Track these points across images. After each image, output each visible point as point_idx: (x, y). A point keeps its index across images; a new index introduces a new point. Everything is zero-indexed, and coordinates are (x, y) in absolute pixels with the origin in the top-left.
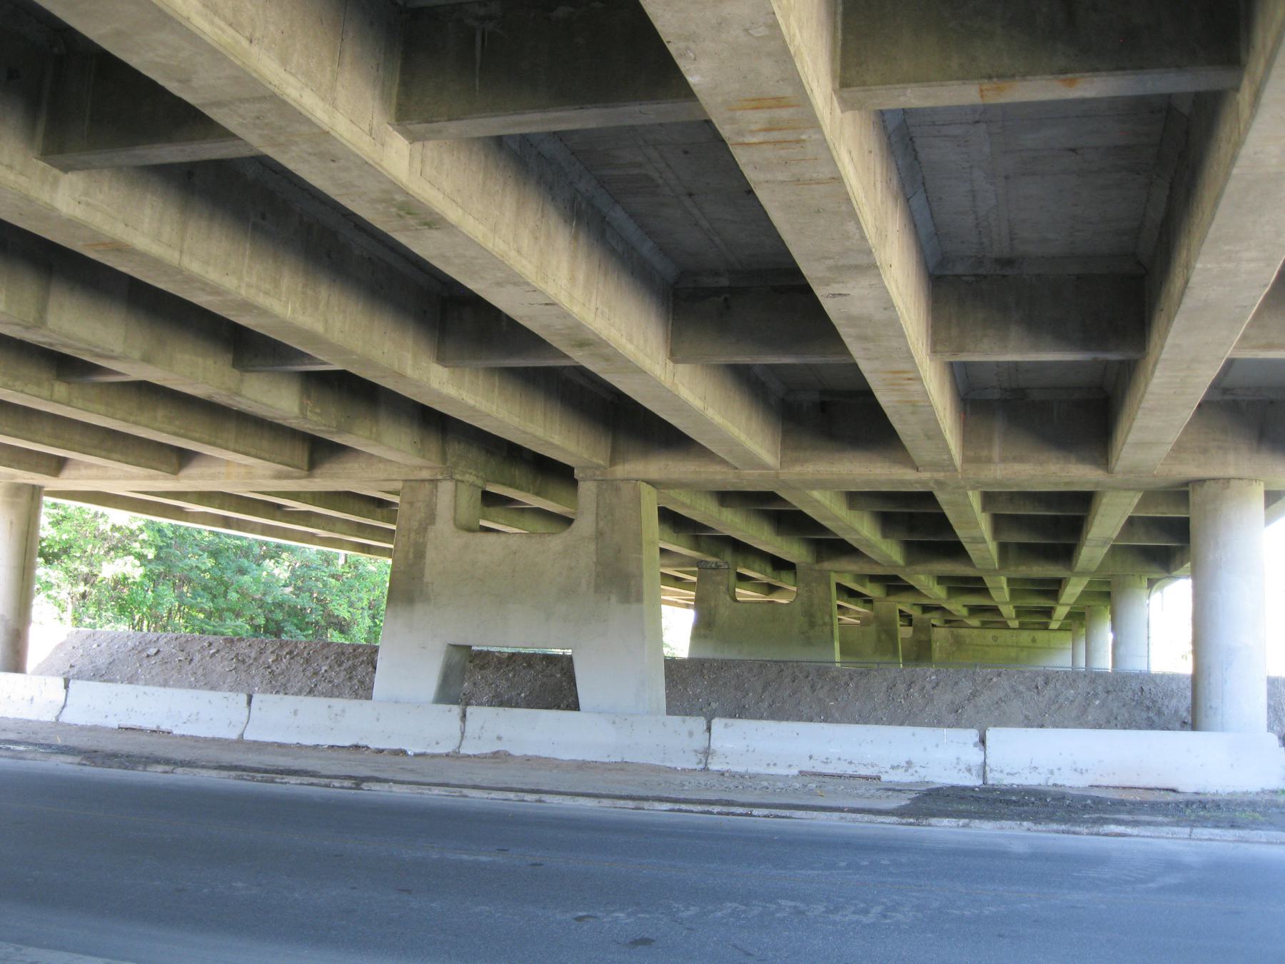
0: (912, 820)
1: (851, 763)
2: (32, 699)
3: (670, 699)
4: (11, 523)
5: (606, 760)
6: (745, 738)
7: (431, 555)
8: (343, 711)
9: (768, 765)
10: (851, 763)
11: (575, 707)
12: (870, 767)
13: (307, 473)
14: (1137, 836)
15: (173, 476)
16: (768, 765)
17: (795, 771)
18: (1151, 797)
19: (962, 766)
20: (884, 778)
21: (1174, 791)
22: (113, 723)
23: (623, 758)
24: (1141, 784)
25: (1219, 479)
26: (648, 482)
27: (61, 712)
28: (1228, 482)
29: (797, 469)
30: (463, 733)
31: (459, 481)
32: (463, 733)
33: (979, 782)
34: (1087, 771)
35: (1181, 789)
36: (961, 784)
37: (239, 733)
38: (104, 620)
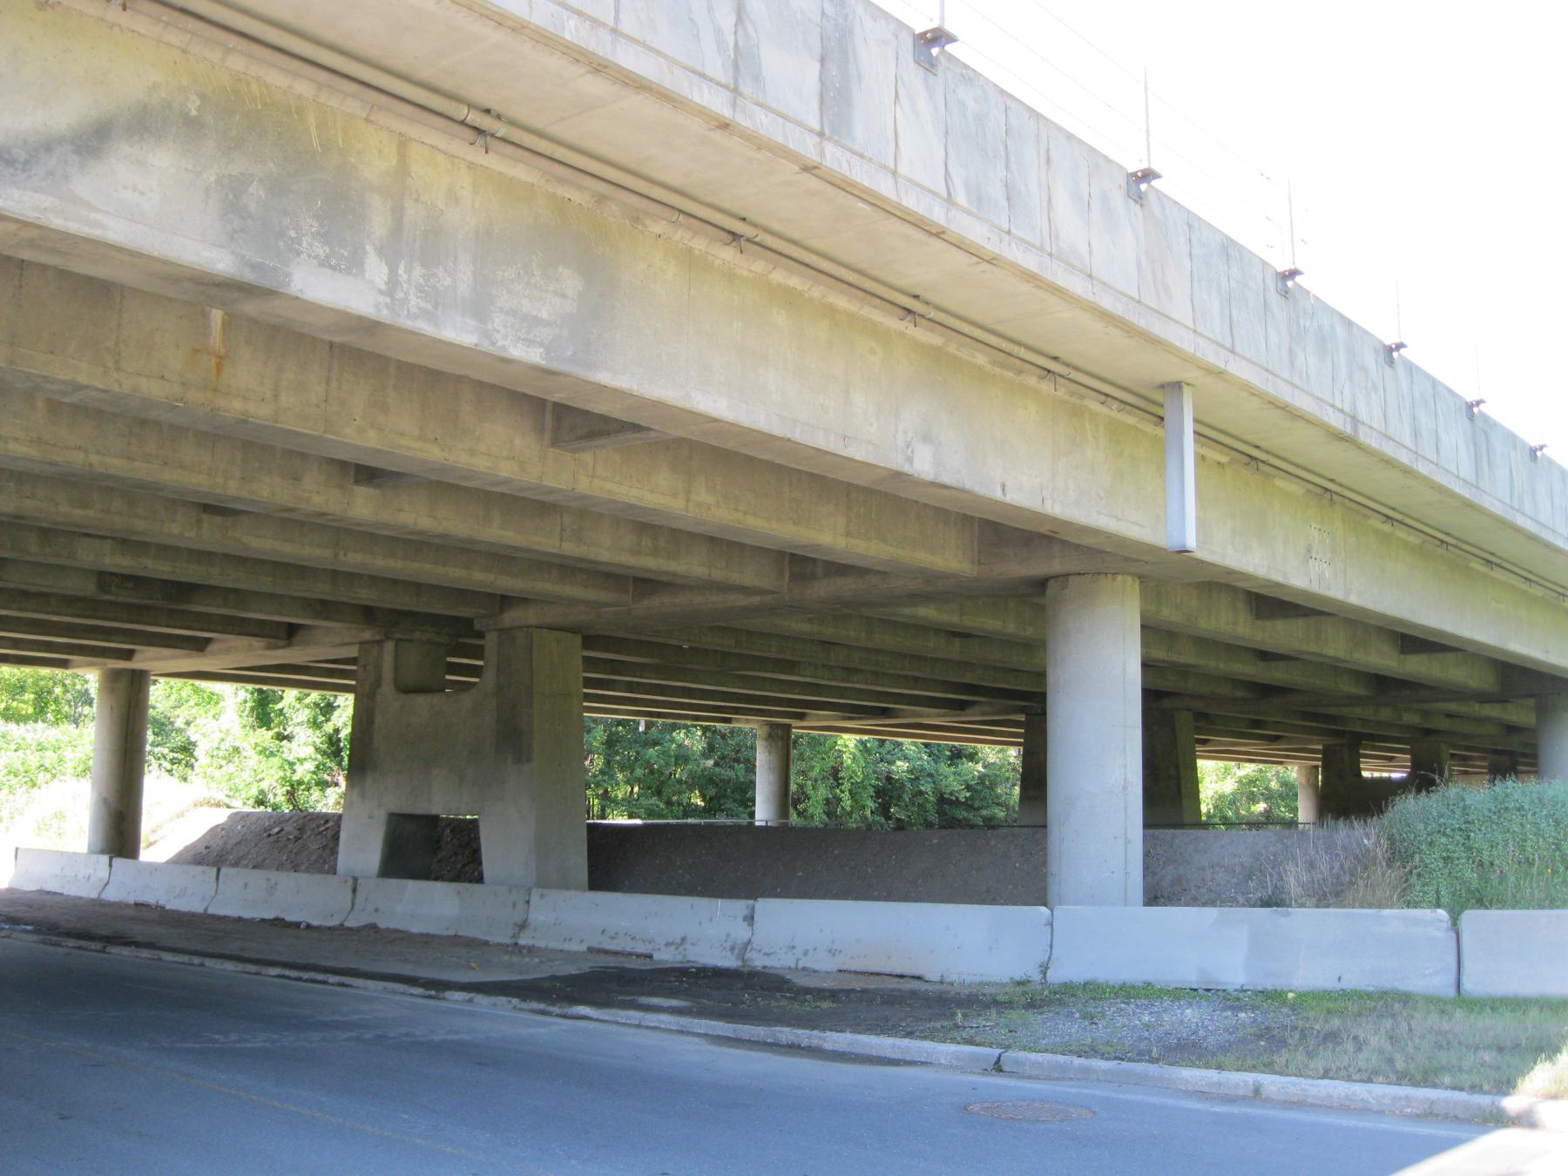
0: (433, 993)
1: (633, 939)
2: (89, 877)
3: (1241, 899)
4: (112, 708)
5: (445, 933)
6: (555, 910)
7: (378, 720)
8: (276, 884)
9: (565, 940)
10: (633, 939)
11: (480, 879)
12: (647, 943)
13: (286, 641)
14: (596, 1020)
15: (199, 653)
16: (565, 940)
17: (584, 948)
18: (873, 984)
19: (728, 945)
20: (656, 956)
21: (919, 978)
22: (131, 899)
23: (457, 932)
24: (887, 970)
25: (1058, 576)
26: (551, 628)
27: (103, 889)
28: (1067, 580)
29: (646, 603)
30: (353, 905)
31: (401, 640)
32: (353, 905)
33: (739, 963)
34: (840, 952)
35: (928, 976)
36: (720, 965)
37: (205, 907)
38: (853, 820)
